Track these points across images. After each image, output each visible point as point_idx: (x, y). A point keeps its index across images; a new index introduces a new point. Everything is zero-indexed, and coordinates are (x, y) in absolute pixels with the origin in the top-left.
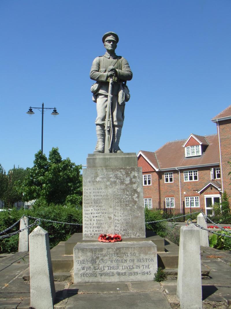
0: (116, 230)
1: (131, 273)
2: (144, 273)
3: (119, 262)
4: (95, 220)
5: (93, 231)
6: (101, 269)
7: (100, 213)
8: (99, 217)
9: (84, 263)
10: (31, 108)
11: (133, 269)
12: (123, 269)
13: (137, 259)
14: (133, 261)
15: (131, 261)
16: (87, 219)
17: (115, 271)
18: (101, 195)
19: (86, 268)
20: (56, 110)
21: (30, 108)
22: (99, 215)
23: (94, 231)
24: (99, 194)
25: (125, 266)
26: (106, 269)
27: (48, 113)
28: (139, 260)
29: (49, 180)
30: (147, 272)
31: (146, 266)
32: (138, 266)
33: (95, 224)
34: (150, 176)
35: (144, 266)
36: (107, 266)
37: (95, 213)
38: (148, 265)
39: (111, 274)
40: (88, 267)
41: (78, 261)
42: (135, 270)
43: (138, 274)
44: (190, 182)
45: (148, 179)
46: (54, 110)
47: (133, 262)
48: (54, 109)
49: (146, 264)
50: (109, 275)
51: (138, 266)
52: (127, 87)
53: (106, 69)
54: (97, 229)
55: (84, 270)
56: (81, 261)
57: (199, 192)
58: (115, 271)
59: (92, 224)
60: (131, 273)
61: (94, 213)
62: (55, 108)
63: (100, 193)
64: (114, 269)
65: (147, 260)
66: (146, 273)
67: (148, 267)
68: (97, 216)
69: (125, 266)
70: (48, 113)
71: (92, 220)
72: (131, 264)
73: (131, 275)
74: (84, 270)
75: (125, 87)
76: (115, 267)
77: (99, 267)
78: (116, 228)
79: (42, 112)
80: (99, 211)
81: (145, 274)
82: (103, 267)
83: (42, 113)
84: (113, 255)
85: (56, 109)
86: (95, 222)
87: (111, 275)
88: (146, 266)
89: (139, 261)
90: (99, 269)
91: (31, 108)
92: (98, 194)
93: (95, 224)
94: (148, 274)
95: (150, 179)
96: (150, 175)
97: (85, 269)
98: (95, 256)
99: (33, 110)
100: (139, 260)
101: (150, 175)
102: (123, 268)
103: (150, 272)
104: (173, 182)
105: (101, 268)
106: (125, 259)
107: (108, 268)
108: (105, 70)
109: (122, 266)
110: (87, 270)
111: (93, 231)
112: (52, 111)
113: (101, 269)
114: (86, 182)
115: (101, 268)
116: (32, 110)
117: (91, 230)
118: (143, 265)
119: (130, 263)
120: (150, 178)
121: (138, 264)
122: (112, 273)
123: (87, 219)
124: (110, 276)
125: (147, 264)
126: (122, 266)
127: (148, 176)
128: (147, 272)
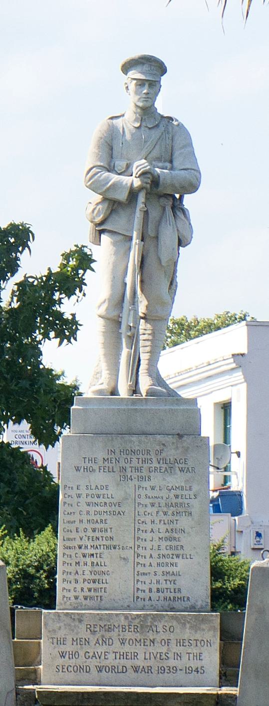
0: (138, 589)
1: (163, 669)
2: (190, 669)
3: (139, 644)
4: (89, 564)
5: (82, 589)
6: (100, 658)
7: (100, 545)
8: (98, 556)
9: (63, 644)
11: (167, 661)
12: (145, 659)
13: (177, 640)
14: (168, 642)
15: (163, 644)
16: (68, 560)
18: (105, 503)
19: (68, 653)
22: (98, 551)
23: (86, 589)
24: (101, 500)
25: (150, 653)
26: (111, 656)
28: (181, 641)
30: (197, 668)
31: (195, 655)
32: (177, 654)
33: (87, 572)
35: (191, 656)
36: (113, 652)
37: (89, 547)
38: (200, 653)
39: (120, 668)
40: (73, 653)
41: (53, 638)
42: (172, 663)
43: (176, 670)
47: (168, 645)
49: (195, 651)
50: (116, 670)
51: (177, 654)
52: (184, 212)
53: (128, 162)
54: (92, 585)
55: (64, 657)
56: (59, 639)
58: (129, 663)
59: (80, 572)
60: (163, 669)
61: (86, 547)
63: (97, 583)
64: (126, 659)
65: (198, 643)
66: (194, 669)
67: (199, 657)
68: (93, 555)
69: (150, 653)
71: (82, 564)
72: (164, 649)
73: (163, 672)
74: (64, 657)
75: (178, 213)
76: (130, 655)
77: (96, 653)
78: (139, 586)
80: (97, 543)
81: (192, 671)
82: (105, 652)
84: (127, 628)
86: (88, 569)
87: (119, 671)
88: (194, 656)
89: (181, 644)
90: (95, 656)
92: (96, 500)
93: (87, 572)
94: (198, 672)
97: (67, 656)
98: (88, 630)
100: (181, 641)
102: (146, 658)
103: (202, 667)
105: (100, 654)
106: (151, 639)
107: (114, 655)
108: (127, 164)
109: (145, 653)
110: (69, 658)
111: (82, 589)
113: (100, 658)
115: (100, 654)
117: (79, 586)
118: (189, 653)
119: (163, 647)
122: (123, 667)
123: (68, 560)
124: (118, 672)
125: (196, 651)
126: (145, 653)
128: (197, 668)
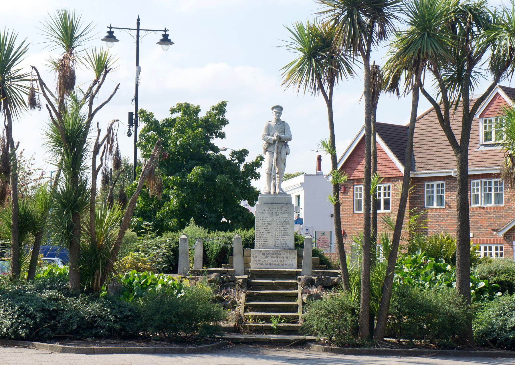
10: (112, 30)
17: (273, 263)
20: (168, 35)
21: (109, 30)
27: (150, 40)
29: (423, 244)
34: (389, 189)
42: (285, 263)
44: (495, 208)
45: (385, 196)
46: (163, 35)
48: (164, 33)
57: (501, 234)
58: (273, 263)
62: (165, 31)
67: (292, 261)
70: (150, 40)
79: (136, 38)
83: (135, 41)
85: (167, 33)
86: (263, 238)
91: (111, 28)
95: (389, 196)
96: (391, 185)
99: (117, 34)
101: (389, 187)
104: (503, 205)
112: (159, 36)
114: (422, 264)
116: (113, 32)
120: (389, 194)
121: (286, 259)
127: (385, 189)
